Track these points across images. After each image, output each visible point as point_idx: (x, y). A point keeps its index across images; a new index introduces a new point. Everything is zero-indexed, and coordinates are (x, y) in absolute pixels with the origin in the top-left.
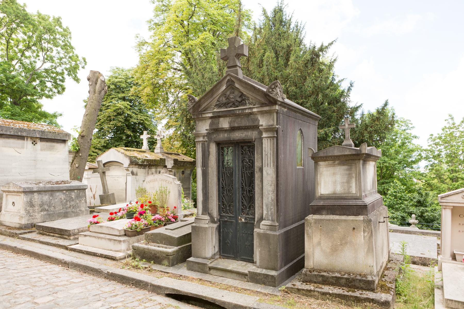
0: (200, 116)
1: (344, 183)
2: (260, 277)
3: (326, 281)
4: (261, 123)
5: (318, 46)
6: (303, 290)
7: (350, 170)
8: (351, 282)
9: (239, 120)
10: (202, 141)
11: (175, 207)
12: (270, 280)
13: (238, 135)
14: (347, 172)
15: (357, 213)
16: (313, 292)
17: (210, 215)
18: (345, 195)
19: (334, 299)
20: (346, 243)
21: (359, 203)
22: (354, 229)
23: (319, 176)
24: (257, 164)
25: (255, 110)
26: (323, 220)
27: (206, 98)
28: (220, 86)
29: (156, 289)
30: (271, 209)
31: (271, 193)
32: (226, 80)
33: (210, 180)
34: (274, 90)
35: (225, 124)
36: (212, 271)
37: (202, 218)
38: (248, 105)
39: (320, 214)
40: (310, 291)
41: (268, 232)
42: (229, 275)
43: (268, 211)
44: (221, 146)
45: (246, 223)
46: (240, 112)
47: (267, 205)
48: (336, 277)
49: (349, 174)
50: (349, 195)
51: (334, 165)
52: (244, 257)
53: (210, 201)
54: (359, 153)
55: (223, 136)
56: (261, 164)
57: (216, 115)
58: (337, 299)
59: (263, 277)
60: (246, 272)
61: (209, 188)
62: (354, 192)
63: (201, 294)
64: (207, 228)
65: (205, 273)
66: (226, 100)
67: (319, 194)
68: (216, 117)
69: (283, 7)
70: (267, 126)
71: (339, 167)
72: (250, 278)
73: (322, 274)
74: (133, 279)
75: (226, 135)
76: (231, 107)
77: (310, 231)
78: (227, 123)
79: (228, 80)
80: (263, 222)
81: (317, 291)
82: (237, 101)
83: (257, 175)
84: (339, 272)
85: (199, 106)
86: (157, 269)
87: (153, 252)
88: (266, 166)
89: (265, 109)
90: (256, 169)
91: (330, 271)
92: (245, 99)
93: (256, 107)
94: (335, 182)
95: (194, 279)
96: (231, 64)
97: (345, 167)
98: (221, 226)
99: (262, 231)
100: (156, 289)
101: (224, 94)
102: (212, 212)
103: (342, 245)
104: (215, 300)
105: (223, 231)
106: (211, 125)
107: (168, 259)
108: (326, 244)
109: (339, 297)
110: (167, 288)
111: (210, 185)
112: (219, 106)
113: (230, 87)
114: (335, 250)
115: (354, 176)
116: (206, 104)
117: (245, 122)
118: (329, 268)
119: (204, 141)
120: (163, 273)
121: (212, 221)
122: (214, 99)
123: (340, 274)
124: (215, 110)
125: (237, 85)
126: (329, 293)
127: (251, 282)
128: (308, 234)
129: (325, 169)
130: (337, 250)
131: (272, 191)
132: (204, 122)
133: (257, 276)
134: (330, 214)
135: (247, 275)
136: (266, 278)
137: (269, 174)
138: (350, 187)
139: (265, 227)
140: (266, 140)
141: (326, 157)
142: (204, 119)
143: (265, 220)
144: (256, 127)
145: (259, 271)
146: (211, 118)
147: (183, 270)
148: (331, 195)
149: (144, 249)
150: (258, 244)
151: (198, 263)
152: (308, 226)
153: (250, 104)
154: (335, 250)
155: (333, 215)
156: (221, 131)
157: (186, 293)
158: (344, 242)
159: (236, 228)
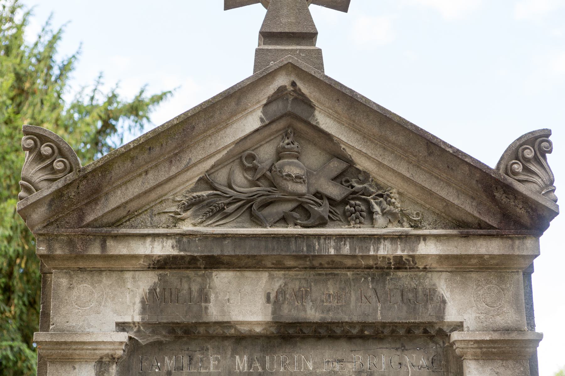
0: (96, 250)
4: (452, 315)
5: (127, 97)
9: (332, 288)
27: (143, 157)
28: (234, 114)
32: (271, 89)
38: (380, 220)
46: (346, 249)
57: (197, 250)
66: (254, 183)
70: (486, 329)
76: (284, 220)
78: (260, 300)
79: (281, 89)
82: (318, 195)
85: (95, 196)
92: (366, 192)
93: (437, 237)
96: (286, 24)
101: (243, 155)
106: (153, 301)
113: (281, 124)
117: (360, 305)
122: (188, 168)
124: (186, 227)
125: (324, 121)
132: (106, 281)
142: (116, 266)
146: (162, 264)
153: (392, 217)
156: (211, 338)
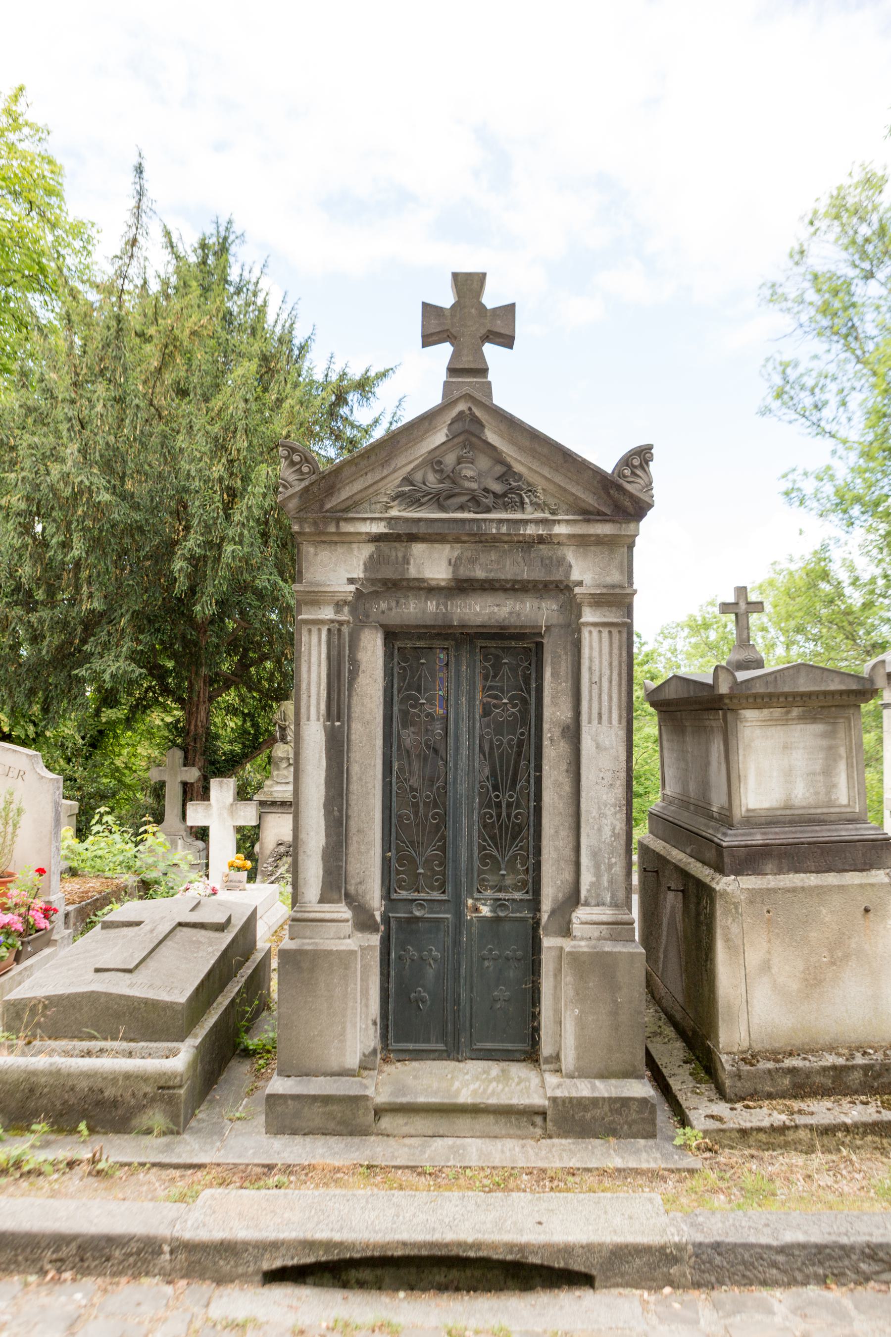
1: (814, 774)
2: (598, 1113)
3: (803, 1086)
4: (575, 576)
6: (760, 1130)
7: (831, 735)
8: (879, 1075)
9: (493, 556)
10: (332, 621)
11: (41, 871)
12: (634, 1116)
13: (479, 610)
14: (825, 743)
15: (865, 864)
16: (791, 1132)
17: (350, 900)
18: (819, 811)
19: (859, 1142)
20: (847, 957)
21: (866, 832)
22: (867, 910)
23: (741, 752)
24: (555, 712)
25: (561, 530)
26: (775, 891)
28: (427, 431)
29: (208, 1262)
30: (610, 866)
31: (610, 811)
33: (355, 769)
34: (638, 472)
35: (433, 564)
36: (386, 1123)
37: (328, 916)
38: (529, 508)
39: (758, 872)
40: (782, 1129)
41: (608, 947)
42: (463, 1123)
43: (598, 875)
44: (398, 644)
45: (497, 920)
46: (504, 530)
47: (595, 855)
48: (834, 1068)
49: (830, 748)
50: (832, 810)
51: (785, 721)
52: (488, 1045)
53: (353, 848)
54: (868, 686)
55: (414, 610)
56: (569, 714)
57: (401, 529)
58: (869, 1138)
59: (606, 1108)
60: (537, 1100)
61: (353, 798)
62: (844, 800)
63: (449, 1236)
64: (352, 953)
65: (362, 1132)
66: (441, 482)
67: (744, 809)
68: (404, 536)
69: (230, 241)
70: (598, 586)
71: (799, 727)
72: (556, 1122)
73: (789, 1063)
74: (59, 1241)
75: (431, 606)
76: (462, 508)
77: (735, 929)
78: (444, 563)
79: (461, 413)
80: (581, 914)
81: (806, 1126)
82: (486, 490)
83: (553, 753)
84: (831, 1049)
86: (136, 1160)
87: (84, 1085)
88: (595, 722)
89: (599, 532)
90: (550, 730)
91: (813, 1051)
93: (567, 521)
94: (788, 774)
95: (338, 1170)
97: (819, 728)
98: (393, 940)
99: (583, 946)
100: (208, 1262)
101: (434, 461)
102: (361, 889)
103: (834, 964)
104: (522, 1248)
105: (400, 958)
106: (371, 564)
107: (171, 1101)
108: (787, 968)
109: (873, 1133)
110: (275, 1246)
111: (354, 787)
112: (412, 499)
113: (461, 439)
114: (814, 982)
115: (844, 755)
116: (358, 486)
117: (513, 568)
118: (797, 1042)
119: (341, 623)
120: (177, 1173)
121: (364, 923)
122: (394, 471)
123: (839, 1055)
124: (394, 513)
125: (491, 437)
126: (845, 1124)
127: (559, 1136)
128: (727, 940)
129: (758, 732)
130: (821, 981)
131: (615, 806)
132: (340, 549)
133: (585, 1109)
134: (789, 871)
135: (543, 1114)
136: (618, 1112)
137: (606, 749)
138: (831, 787)
139: (594, 931)
140: (595, 634)
141: (771, 696)
142: (347, 540)
143: (587, 904)
144: (560, 589)
145: (584, 1089)
146: (377, 538)
147: (245, 1139)
148: (779, 812)
149: (34, 1073)
150: (571, 993)
151: (326, 1100)
152: (727, 912)
153: (537, 506)
154: (814, 982)
155: (797, 872)
157: (375, 1246)
158: (839, 954)
159: (457, 943)
